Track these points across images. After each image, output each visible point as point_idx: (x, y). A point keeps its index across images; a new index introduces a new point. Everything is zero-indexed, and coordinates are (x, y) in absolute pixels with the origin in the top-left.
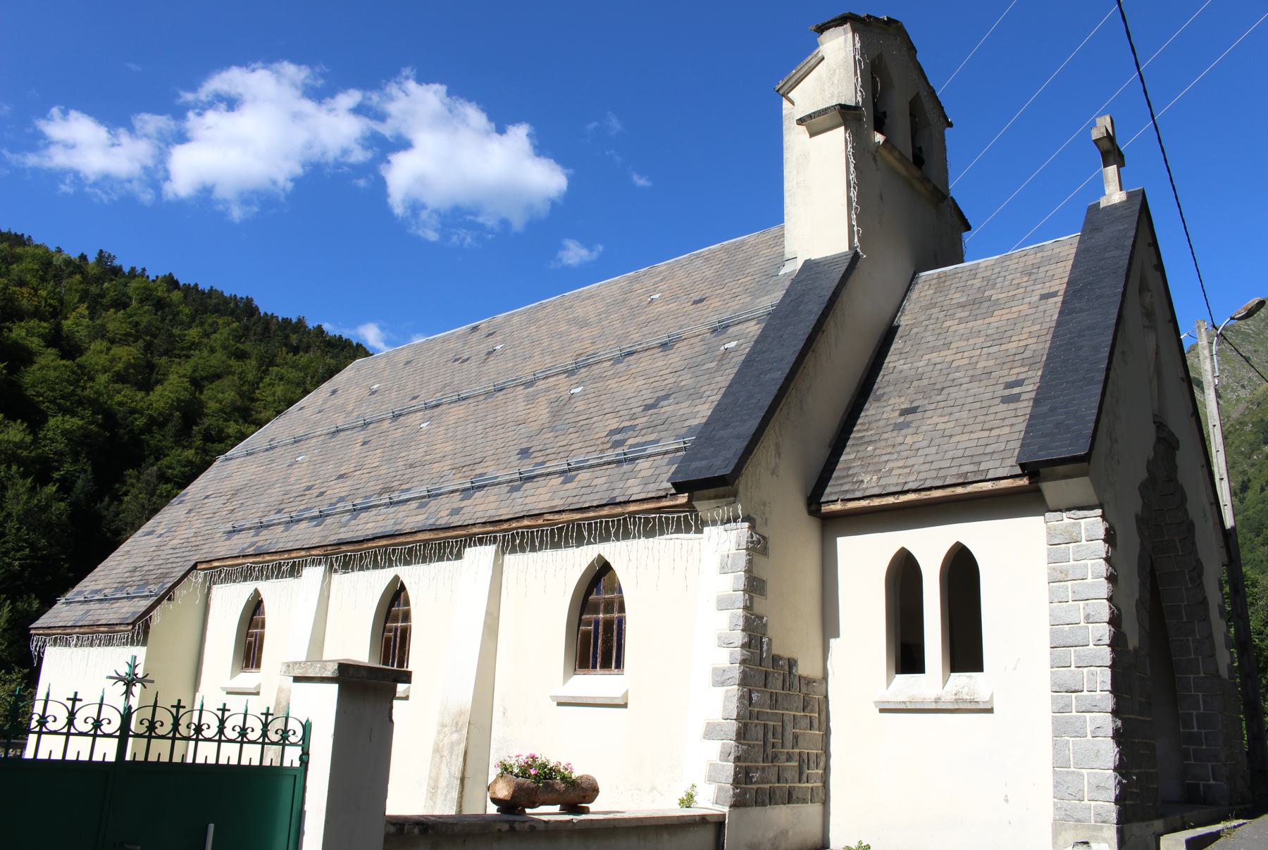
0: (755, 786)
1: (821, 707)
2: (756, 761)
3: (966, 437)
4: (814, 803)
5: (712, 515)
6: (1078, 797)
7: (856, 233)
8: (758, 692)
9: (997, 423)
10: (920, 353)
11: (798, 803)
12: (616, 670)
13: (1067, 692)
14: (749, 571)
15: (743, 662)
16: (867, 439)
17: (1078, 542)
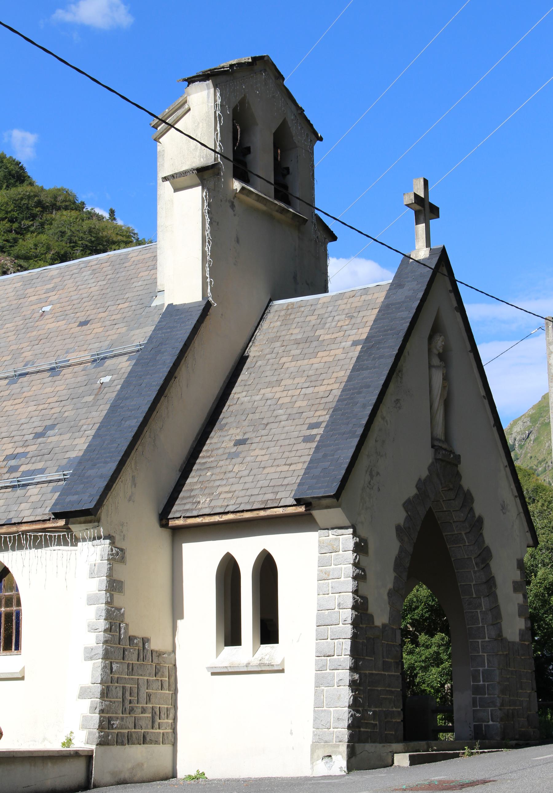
0: (116, 731)
1: (170, 672)
2: (116, 713)
3: (273, 470)
4: (165, 744)
5: (83, 535)
6: (327, 726)
7: (209, 283)
8: (117, 663)
9: (296, 459)
10: (259, 387)
11: (151, 744)
12: (16, 651)
13: (324, 656)
14: (110, 576)
15: (106, 642)
16: (208, 465)
17: (337, 552)
